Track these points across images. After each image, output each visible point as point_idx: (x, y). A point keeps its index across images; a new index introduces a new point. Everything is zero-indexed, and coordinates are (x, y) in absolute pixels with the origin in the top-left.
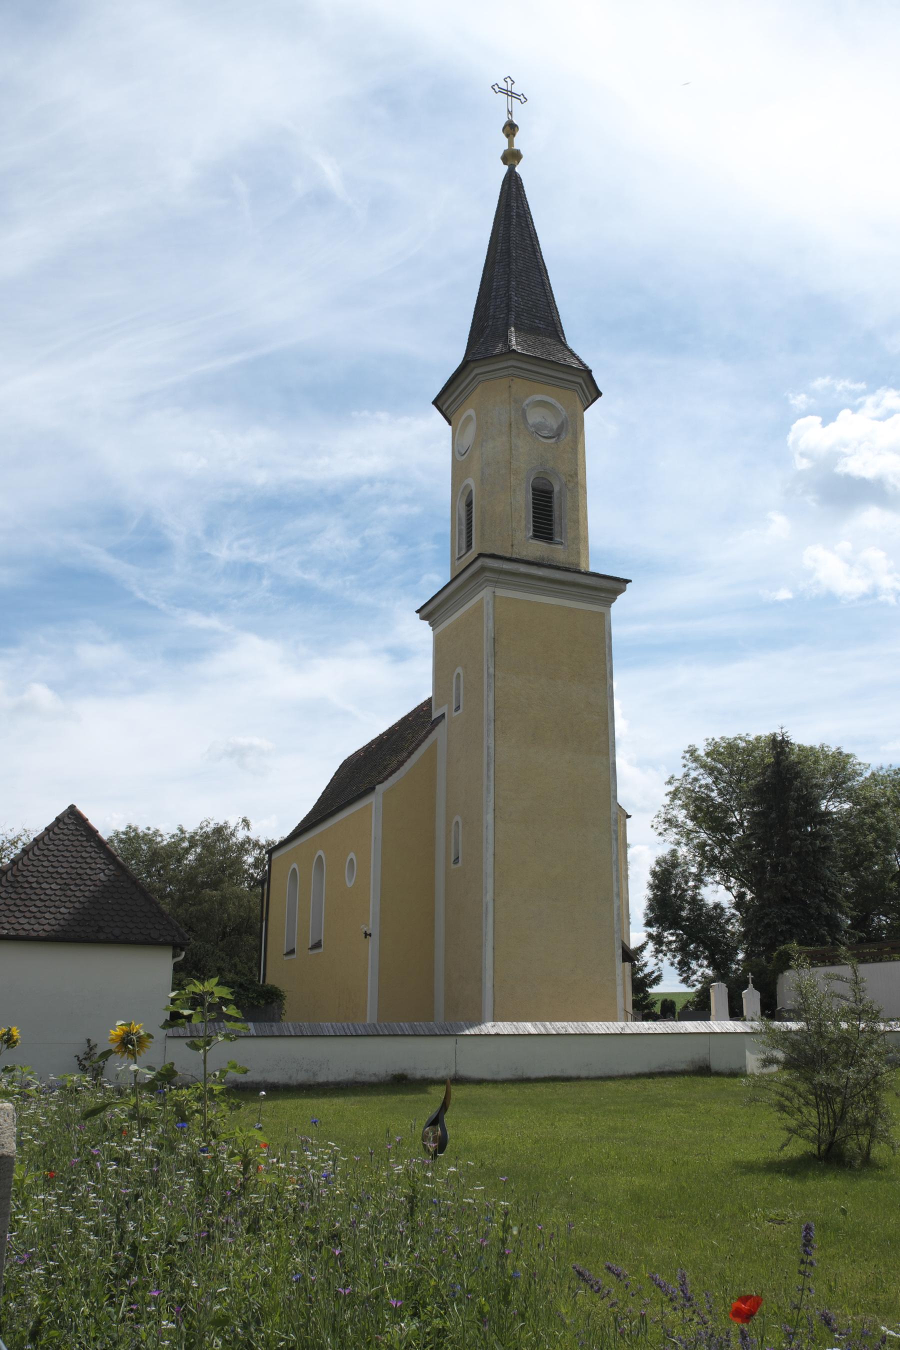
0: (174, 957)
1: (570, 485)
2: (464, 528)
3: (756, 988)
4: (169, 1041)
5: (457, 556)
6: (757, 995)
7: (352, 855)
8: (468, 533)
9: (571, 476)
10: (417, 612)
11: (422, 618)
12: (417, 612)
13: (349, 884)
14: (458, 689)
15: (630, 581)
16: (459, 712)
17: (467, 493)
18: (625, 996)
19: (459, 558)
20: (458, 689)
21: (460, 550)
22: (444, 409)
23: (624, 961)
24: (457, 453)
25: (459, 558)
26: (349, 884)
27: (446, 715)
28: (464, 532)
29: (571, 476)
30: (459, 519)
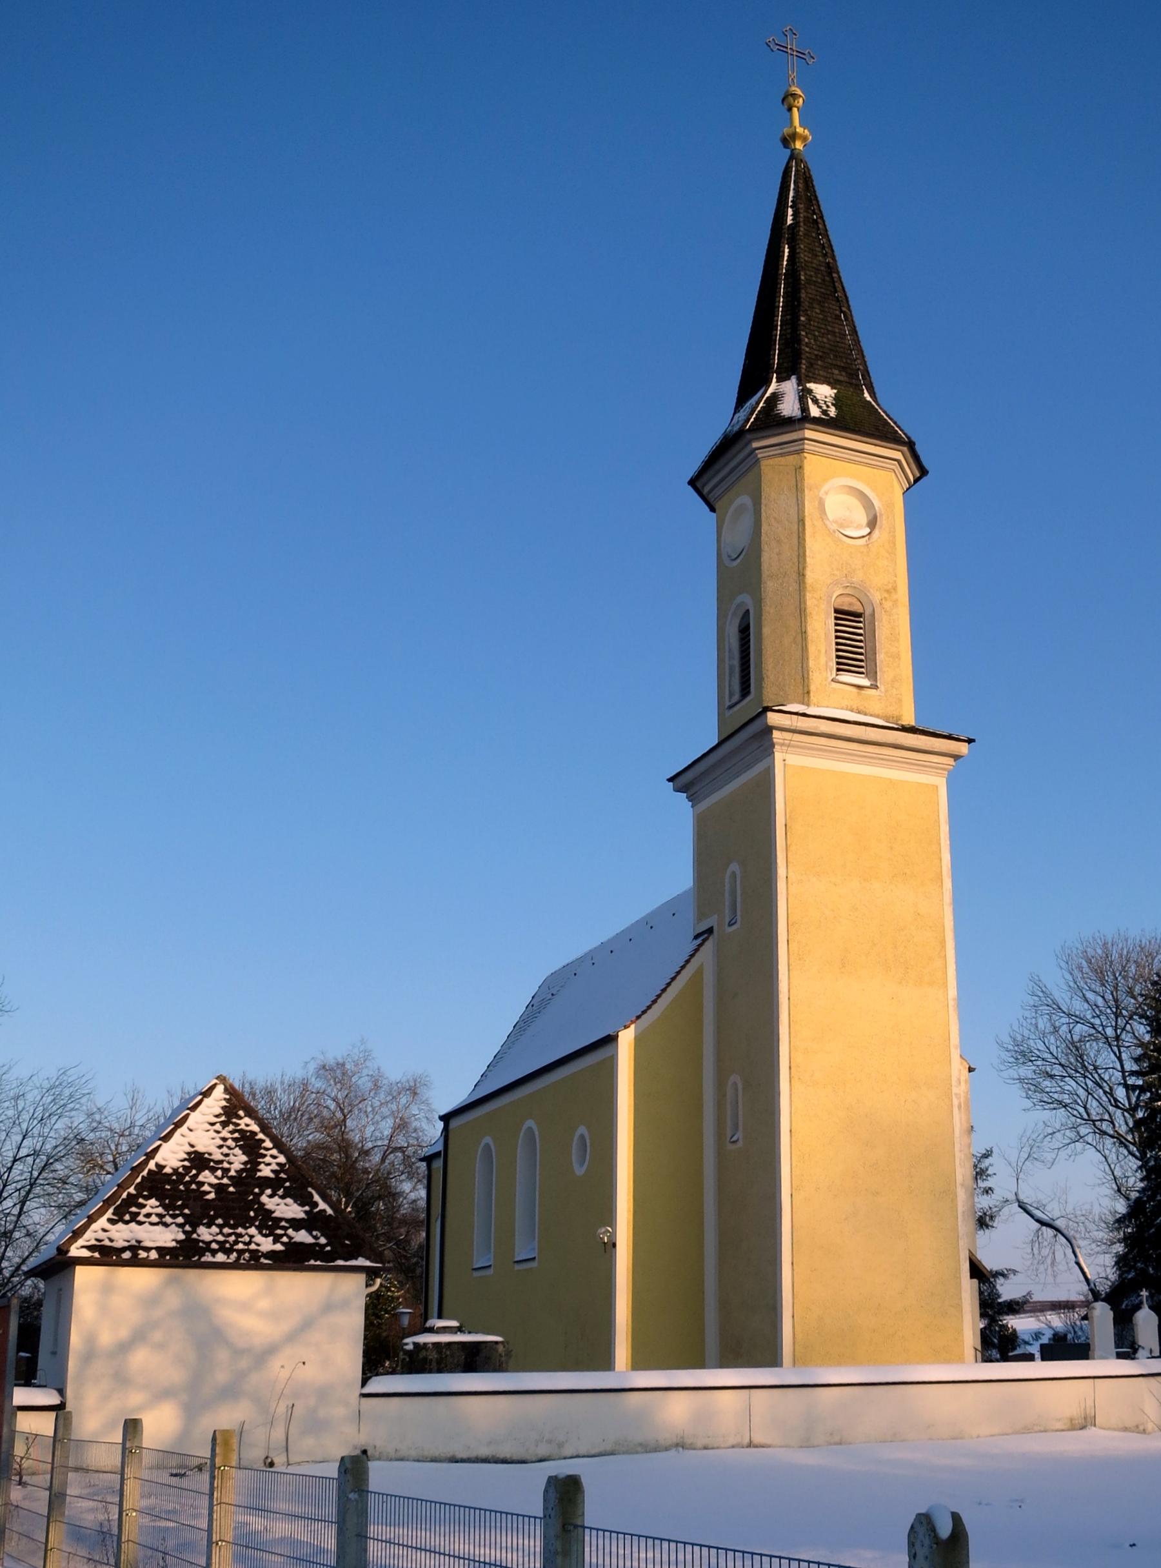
0: (367, 1286)
1: (888, 605)
2: (736, 662)
3: (1150, 1308)
4: (364, 1400)
5: (728, 704)
6: (1154, 1318)
7: (582, 1130)
8: (742, 671)
9: (888, 591)
10: (670, 780)
11: (677, 790)
12: (670, 780)
13: (580, 1171)
14: (733, 893)
15: (1015, 1272)
16: (734, 927)
17: (740, 613)
18: (970, 1326)
19: (730, 707)
20: (733, 893)
21: (731, 695)
22: (706, 490)
23: (972, 1277)
24: (725, 557)
25: (730, 707)
26: (580, 1171)
27: (715, 929)
28: (737, 670)
29: (888, 591)
30: (730, 650)
